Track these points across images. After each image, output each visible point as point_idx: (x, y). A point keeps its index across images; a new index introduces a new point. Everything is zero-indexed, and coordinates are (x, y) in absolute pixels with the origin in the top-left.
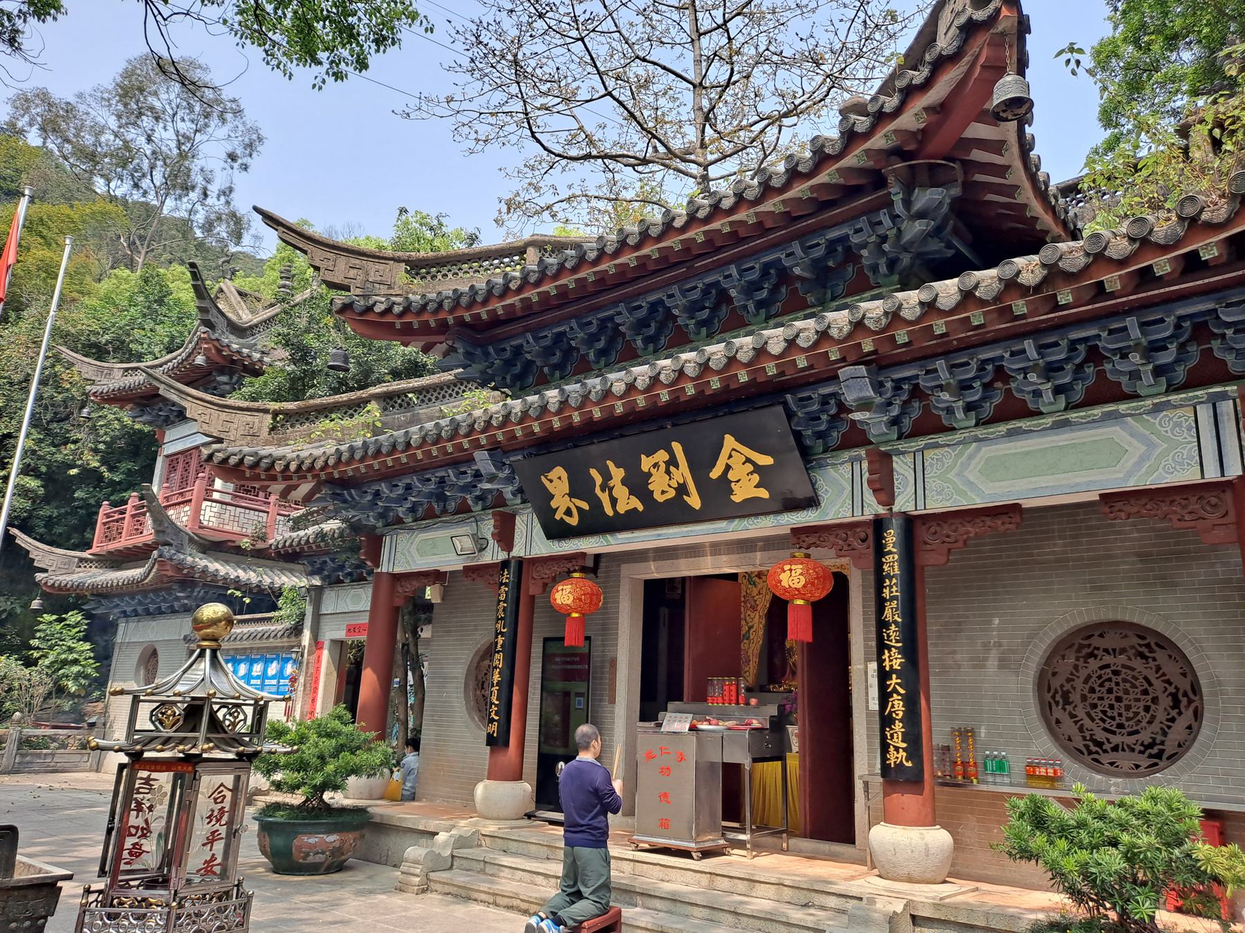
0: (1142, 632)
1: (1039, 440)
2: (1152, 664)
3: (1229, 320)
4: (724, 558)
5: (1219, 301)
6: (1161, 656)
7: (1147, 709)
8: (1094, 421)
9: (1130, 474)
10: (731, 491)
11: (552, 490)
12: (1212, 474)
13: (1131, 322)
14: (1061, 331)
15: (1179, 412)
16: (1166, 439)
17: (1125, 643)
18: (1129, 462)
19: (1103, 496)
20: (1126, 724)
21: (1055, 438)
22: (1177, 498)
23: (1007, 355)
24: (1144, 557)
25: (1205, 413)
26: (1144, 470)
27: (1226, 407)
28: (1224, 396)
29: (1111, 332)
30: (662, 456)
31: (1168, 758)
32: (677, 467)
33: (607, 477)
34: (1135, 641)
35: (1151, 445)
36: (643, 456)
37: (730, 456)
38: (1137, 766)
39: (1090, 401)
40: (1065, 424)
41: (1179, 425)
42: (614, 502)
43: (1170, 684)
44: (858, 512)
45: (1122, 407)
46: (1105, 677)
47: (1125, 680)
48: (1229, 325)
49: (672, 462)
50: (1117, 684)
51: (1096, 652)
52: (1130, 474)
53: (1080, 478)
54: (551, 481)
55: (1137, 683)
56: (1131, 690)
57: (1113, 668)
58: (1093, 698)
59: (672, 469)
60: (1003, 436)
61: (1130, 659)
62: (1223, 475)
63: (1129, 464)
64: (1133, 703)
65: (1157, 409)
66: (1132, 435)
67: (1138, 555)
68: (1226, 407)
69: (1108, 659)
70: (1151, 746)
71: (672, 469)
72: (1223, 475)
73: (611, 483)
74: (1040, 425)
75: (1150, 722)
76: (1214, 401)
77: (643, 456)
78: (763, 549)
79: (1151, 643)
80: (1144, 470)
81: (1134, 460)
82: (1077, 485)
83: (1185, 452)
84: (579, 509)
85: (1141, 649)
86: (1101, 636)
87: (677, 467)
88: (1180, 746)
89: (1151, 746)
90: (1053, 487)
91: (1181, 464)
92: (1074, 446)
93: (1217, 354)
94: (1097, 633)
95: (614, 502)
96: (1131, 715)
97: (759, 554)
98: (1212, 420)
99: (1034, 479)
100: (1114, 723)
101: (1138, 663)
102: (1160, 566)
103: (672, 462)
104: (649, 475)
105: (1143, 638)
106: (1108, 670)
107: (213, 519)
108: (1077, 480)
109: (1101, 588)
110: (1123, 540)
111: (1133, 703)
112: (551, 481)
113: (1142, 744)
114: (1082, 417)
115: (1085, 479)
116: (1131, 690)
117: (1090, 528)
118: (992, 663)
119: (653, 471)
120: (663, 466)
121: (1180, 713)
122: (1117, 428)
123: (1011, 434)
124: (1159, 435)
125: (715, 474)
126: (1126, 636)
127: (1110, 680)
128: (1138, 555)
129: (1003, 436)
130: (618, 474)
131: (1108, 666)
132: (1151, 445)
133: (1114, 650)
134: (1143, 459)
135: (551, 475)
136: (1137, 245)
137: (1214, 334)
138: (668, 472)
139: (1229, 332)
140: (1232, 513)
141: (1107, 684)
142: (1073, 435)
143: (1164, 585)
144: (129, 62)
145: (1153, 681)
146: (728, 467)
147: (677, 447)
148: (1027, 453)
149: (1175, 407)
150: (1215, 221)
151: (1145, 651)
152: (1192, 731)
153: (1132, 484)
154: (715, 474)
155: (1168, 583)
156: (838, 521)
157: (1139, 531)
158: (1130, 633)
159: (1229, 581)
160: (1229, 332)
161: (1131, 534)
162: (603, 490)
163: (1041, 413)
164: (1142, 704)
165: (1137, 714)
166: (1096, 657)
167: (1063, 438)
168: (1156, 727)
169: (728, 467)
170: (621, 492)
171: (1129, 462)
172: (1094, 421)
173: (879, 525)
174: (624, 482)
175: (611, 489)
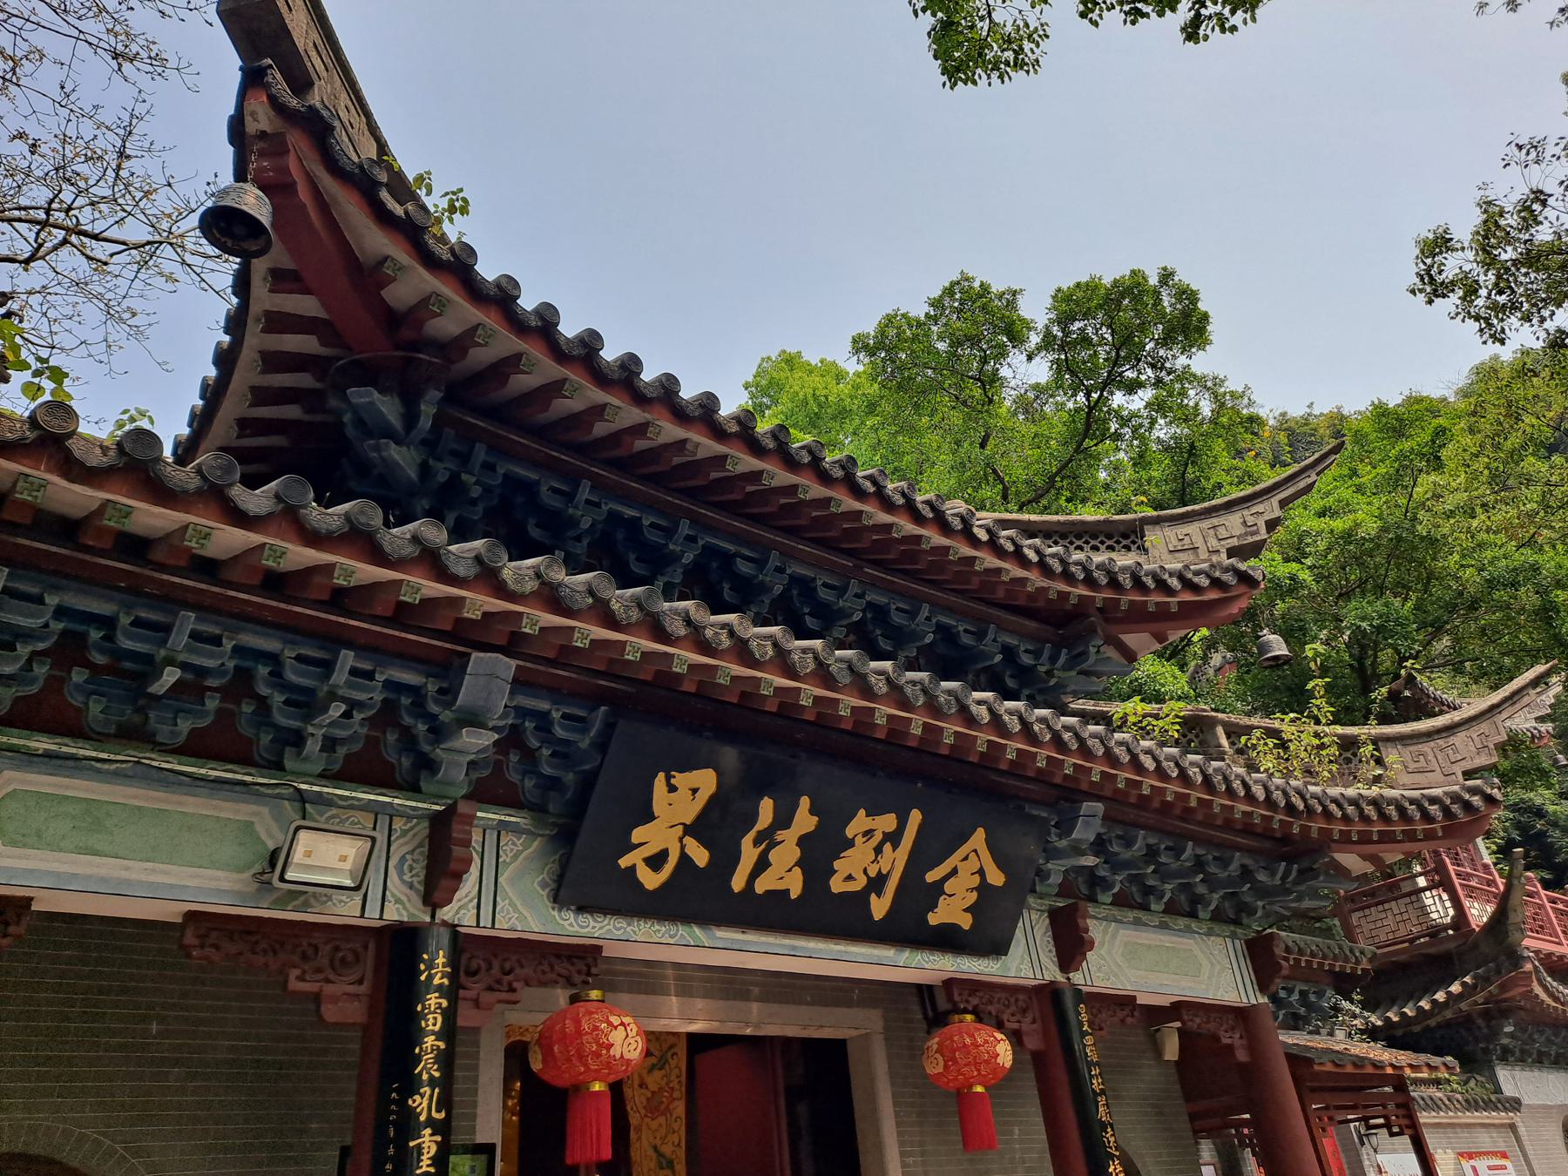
4: (700, 1004)
10: (933, 906)
11: (657, 808)
19: (191, 916)
23: (125, 620)
30: (888, 822)
32: (895, 847)
33: (783, 819)
36: (862, 812)
37: (966, 858)
42: (762, 865)
44: (373, 911)
49: (894, 838)
53: (137, 872)
54: (672, 789)
59: (888, 847)
71: (888, 847)
73: (781, 835)
77: (862, 812)
78: (764, 998)
84: (684, 859)
87: (895, 847)
95: (762, 865)
97: (755, 1006)
103: (894, 838)
104: (850, 844)
107: (1430, 901)
112: (672, 789)
119: (859, 840)
120: (878, 837)
125: (931, 877)
130: (804, 821)
135: (679, 779)
136: (31, 435)
138: (878, 850)
144: (1166, 276)
146: (954, 872)
147: (916, 817)
154: (931, 877)
156: (1003, 980)
160: (278, 698)
162: (756, 843)
169: (954, 872)
170: (786, 852)
173: (402, 944)
174: (803, 841)
175: (773, 844)
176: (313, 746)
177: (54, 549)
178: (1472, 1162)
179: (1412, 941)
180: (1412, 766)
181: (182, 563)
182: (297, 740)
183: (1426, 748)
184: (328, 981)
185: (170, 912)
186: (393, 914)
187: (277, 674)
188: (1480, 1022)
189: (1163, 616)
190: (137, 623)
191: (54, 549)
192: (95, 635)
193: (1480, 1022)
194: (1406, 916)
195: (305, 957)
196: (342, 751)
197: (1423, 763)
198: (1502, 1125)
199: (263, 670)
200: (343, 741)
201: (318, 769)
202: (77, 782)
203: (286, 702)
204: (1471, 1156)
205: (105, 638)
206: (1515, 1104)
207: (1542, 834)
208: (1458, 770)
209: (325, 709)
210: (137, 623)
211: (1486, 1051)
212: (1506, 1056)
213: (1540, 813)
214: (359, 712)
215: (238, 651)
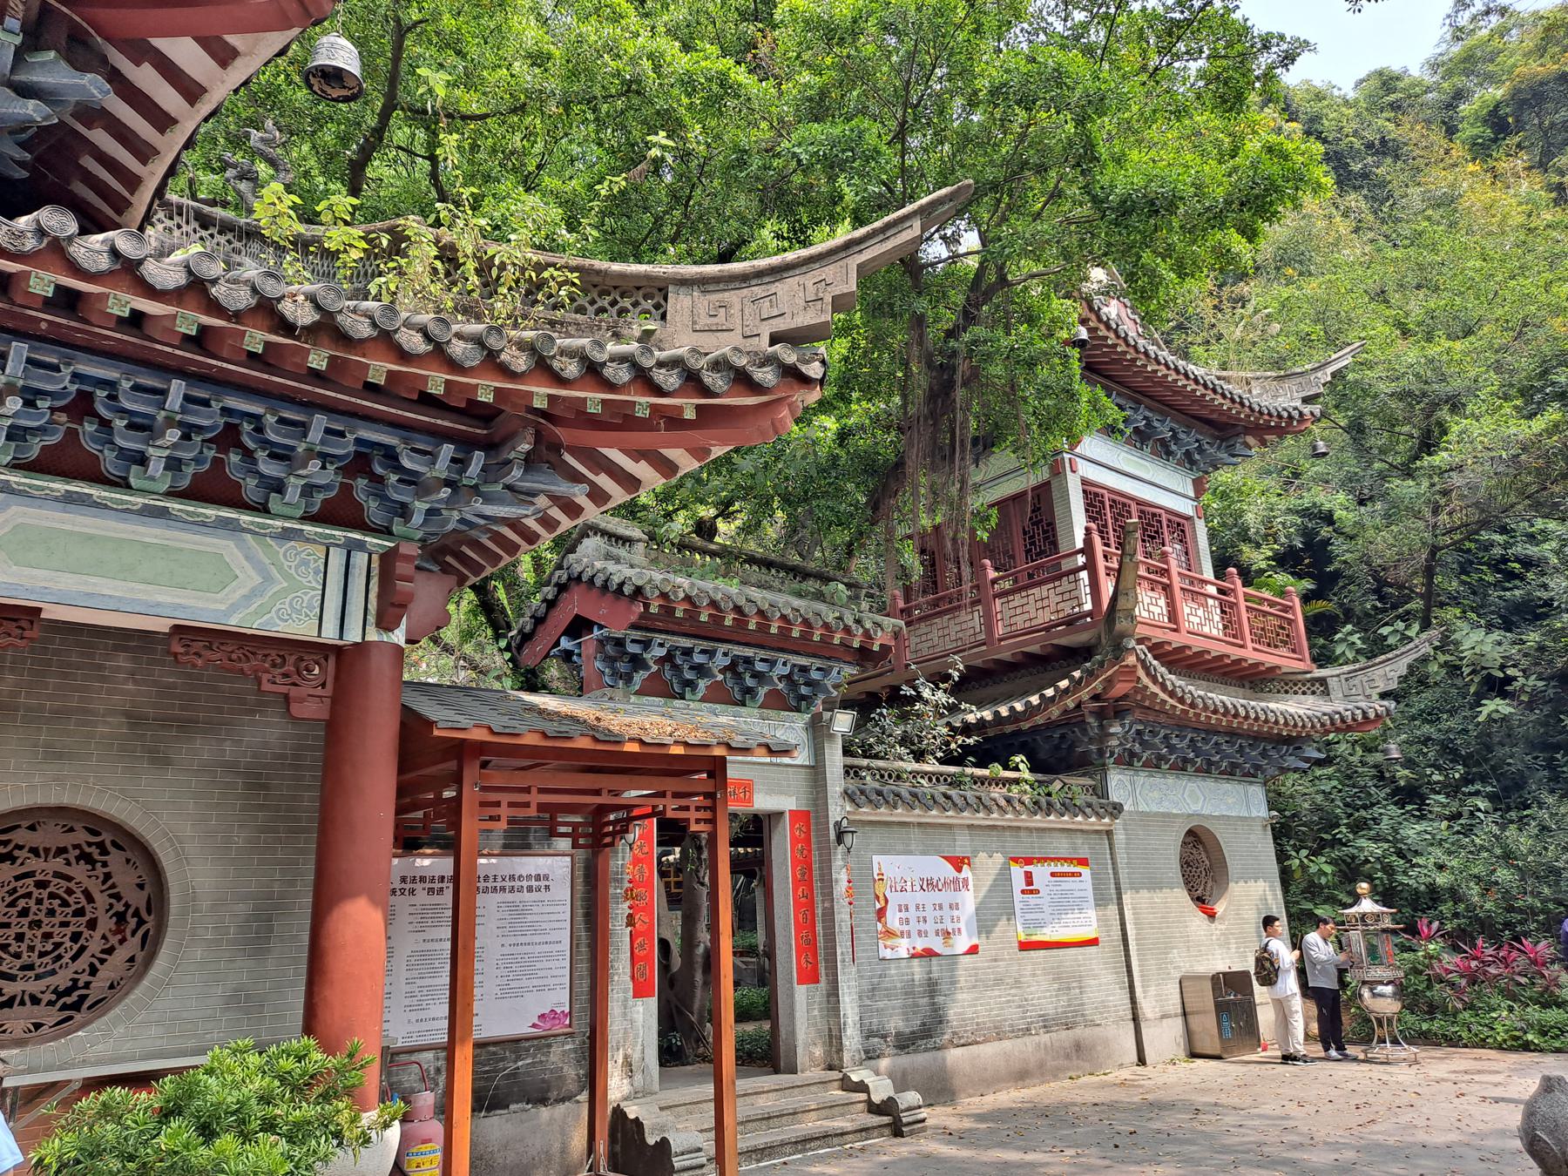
0: (95, 823)
1: (113, 524)
2: (100, 871)
3: (128, 405)
5: (406, 441)
6: (115, 859)
7: (75, 937)
8: (204, 524)
9: (234, 608)
12: (330, 634)
13: (177, 388)
14: (219, 389)
15: (310, 548)
16: (288, 577)
17: (67, 840)
18: (236, 592)
19: (178, 629)
20: (38, 962)
21: (141, 529)
22: (273, 653)
23: (126, 385)
24: (135, 719)
25: (337, 558)
26: (252, 609)
27: (360, 559)
28: (361, 546)
29: (282, 421)
31: (89, 1008)
34: (81, 837)
35: (268, 579)
38: (37, 1026)
39: (197, 493)
40: (163, 513)
41: (305, 563)
43: (118, 897)
45: (246, 518)
46: (21, 892)
47: (52, 896)
48: (123, 412)
50: (39, 902)
51: (16, 853)
52: (234, 608)
55: (71, 900)
56: (59, 910)
57: (39, 877)
58: (79, 924)
60: (56, 499)
61: (68, 863)
62: (341, 638)
63: (237, 595)
64: (56, 930)
65: (286, 535)
66: (247, 558)
67: (127, 714)
68: (360, 559)
69: (34, 864)
70: (68, 992)
72: (341, 638)
74: (123, 502)
75: (74, 959)
76: (351, 548)
79: (104, 839)
80: (252, 609)
81: (244, 591)
82: (158, 605)
83: (306, 599)
85: (88, 850)
86: (32, 828)
88: (112, 987)
89: (68, 992)
90: (120, 599)
91: (299, 612)
92: (164, 548)
93: (360, 497)
94: (25, 824)
96: (49, 947)
98: (343, 569)
99: (94, 580)
100: (18, 963)
101: (79, 871)
102: (153, 734)
105: (95, 833)
106: (30, 881)
108: (160, 598)
109: (60, 756)
110: (109, 692)
111: (56, 930)
113: (55, 991)
114: (187, 513)
115: (168, 599)
116: (59, 910)
117: (69, 665)
118: (628, 903)
121: (122, 941)
122: (231, 544)
123: (69, 499)
124: (280, 570)
126: (71, 830)
127: (28, 895)
128: (127, 714)
129: (56, 499)
131: (30, 874)
132: (268, 579)
133: (47, 850)
134: (254, 593)
136: (430, 348)
137: (96, 415)
139: (120, 424)
140: (329, 685)
141: (22, 903)
142: (168, 533)
143: (153, 761)
145: (97, 895)
148: (91, 537)
149: (308, 540)
150: (86, 266)
151: (94, 851)
152: (139, 966)
153: (234, 623)
155: (160, 760)
157: (136, 682)
158: (78, 826)
159: (235, 764)
160: (120, 424)
161: (125, 685)
163: (129, 486)
164: (68, 931)
165: (57, 945)
166: (13, 860)
167: (152, 533)
168: (83, 962)
171: (236, 592)
172: (204, 524)
176: (156, 467)
177: (125, 338)
178: (1028, 868)
179: (1047, 629)
180: (704, 321)
181: (415, 397)
182: (279, 487)
183: (733, 297)
184: (295, 684)
185: (163, 626)
186: (353, 635)
187: (259, 429)
188: (1091, 720)
189: (1268, 429)
190: (137, 388)
191: (125, 338)
192: (101, 394)
193: (1091, 720)
194: (1039, 604)
195: (274, 665)
196: (319, 497)
197: (721, 318)
198: (1097, 832)
199: (101, 394)
200: (319, 487)
201: (164, 488)
202: (98, 520)
203: (399, 481)
204: (1029, 861)
205: (109, 397)
206: (1117, 809)
207: (1327, 542)
208: (766, 331)
209: (163, 435)
210: (137, 388)
211: (1101, 753)
212: (1127, 760)
213: (1328, 518)
214: (198, 434)
215: (359, 441)
